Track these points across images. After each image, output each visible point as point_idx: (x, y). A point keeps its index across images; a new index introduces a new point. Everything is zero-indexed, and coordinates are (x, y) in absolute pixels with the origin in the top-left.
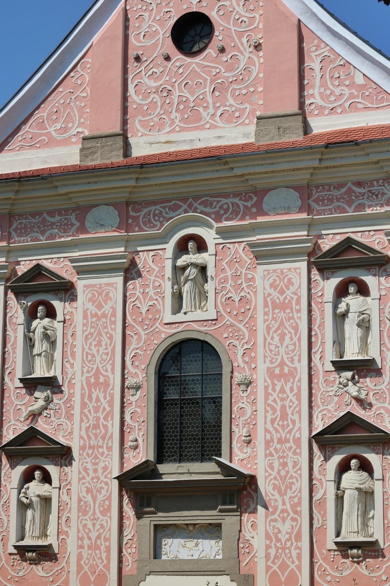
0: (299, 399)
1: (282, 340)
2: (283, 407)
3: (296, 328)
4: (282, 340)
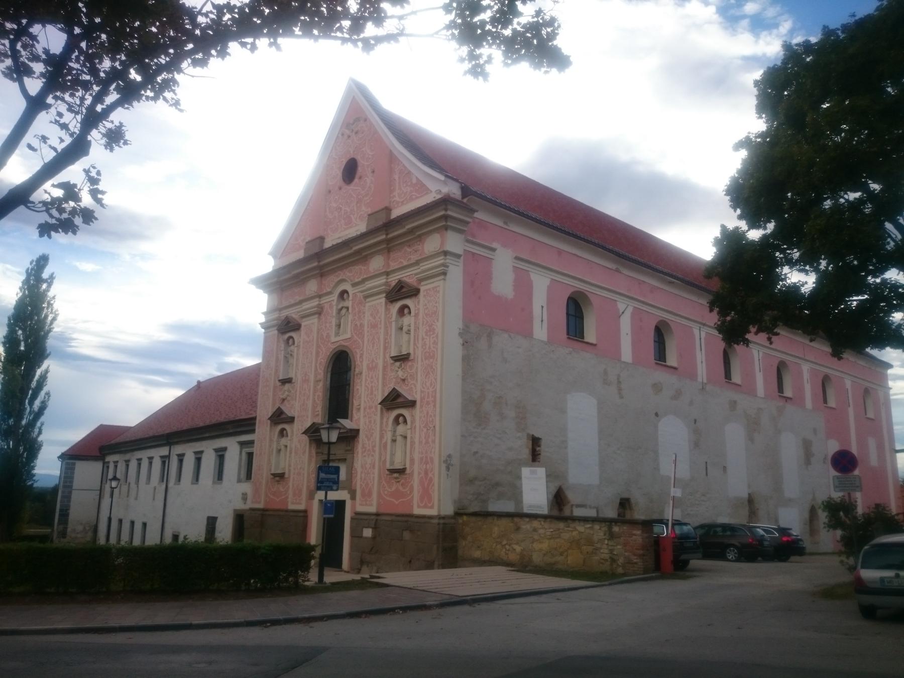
3: (379, 339)
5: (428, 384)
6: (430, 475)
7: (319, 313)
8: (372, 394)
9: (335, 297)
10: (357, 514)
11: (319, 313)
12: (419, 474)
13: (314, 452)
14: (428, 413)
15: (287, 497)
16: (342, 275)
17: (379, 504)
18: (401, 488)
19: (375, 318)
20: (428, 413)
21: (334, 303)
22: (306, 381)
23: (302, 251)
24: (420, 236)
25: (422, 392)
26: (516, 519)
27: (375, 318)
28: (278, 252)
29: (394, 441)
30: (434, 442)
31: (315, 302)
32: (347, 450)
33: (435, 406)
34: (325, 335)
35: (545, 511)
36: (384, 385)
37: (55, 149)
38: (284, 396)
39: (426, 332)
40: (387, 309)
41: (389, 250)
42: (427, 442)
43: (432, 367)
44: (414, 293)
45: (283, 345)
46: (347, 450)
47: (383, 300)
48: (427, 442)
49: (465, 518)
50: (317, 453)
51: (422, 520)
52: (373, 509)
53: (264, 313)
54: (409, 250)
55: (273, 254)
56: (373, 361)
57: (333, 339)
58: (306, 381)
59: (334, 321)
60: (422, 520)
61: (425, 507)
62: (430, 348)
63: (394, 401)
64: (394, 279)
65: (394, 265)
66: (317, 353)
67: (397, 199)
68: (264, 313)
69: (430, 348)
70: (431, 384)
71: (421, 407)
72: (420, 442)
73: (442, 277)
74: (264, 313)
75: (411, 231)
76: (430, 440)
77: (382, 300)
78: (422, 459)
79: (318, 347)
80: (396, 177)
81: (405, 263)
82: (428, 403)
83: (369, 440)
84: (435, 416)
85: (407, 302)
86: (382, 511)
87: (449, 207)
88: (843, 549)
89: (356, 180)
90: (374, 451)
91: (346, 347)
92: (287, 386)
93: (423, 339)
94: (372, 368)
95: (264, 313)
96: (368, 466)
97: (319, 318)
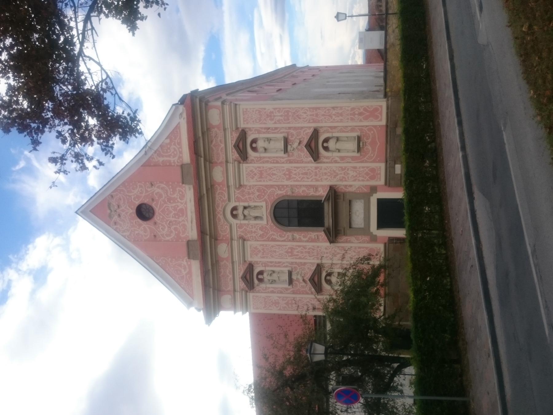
0: (299, 167)
1: (275, 174)
2: (302, 174)
3: (270, 169)
4: (275, 174)
5: (305, 116)
6: (362, 110)
7: (244, 240)
8: (306, 174)
10: (386, 184)
11: (244, 240)
12: (361, 121)
13: (344, 238)
14: (323, 115)
15: (375, 127)
16: (219, 209)
17: (380, 161)
18: (370, 140)
19: (255, 174)
20: (323, 115)
25: (309, 122)
26: (388, 47)
27: (255, 174)
28: (189, 301)
29: (339, 151)
30: (341, 108)
31: (235, 243)
32: (344, 200)
33: (319, 108)
34: (261, 233)
35: (383, 32)
37: (123, 113)
39: (272, 120)
40: (252, 162)
41: (210, 162)
42: (341, 115)
43: (294, 113)
46: (344, 200)
48: (341, 115)
49: (388, 90)
51: (389, 115)
52: (383, 166)
53: (235, 312)
55: (190, 304)
60: (389, 115)
61: (381, 113)
62: (281, 116)
63: (314, 146)
66: (274, 240)
67: (176, 158)
68: (235, 313)
69: (281, 116)
70: (305, 113)
71: (319, 122)
72: (341, 121)
73: (238, 106)
74: (235, 312)
75: (203, 133)
76: (340, 112)
78: (352, 119)
80: (161, 159)
81: (223, 145)
82: (317, 115)
83: (337, 175)
84: (325, 108)
86: (384, 158)
88: (413, 395)
89: (153, 205)
90: (345, 167)
91: (271, 206)
93: (275, 123)
94: (289, 175)
95: (235, 313)
96: (355, 174)
97: (248, 240)
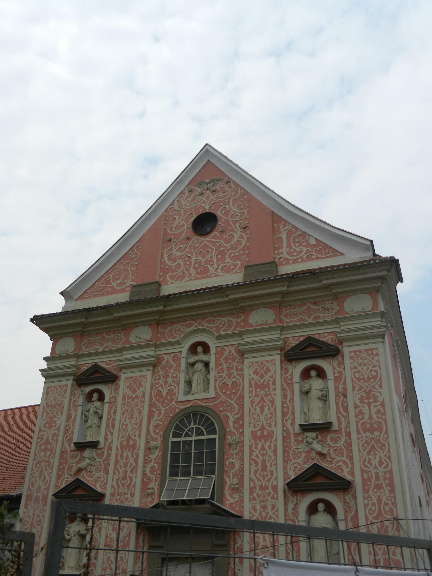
3: (273, 402)
8: (264, 468)
9: (185, 348)
14: (379, 500)
21: (184, 354)
22: (129, 445)
23: (128, 294)
24: (125, 325)
31: (150, 352)
36: (59, 477)
38: (82, 465)
41: (82, 334)
44: (111, 379)
45: (81, 401)
47: (277, 358)
50: (150, 547)
54: (106, 336)
56: (263, 428)
57: (181, 397)
58: (129, 445)
59: (182, 378)
62: (371, 417)
64: (87, 363)
65: (85, 350)
66: (151, 415)
69: (371, 417)
70: (381, 463)
77: (69, 382)
79: (152, 405)
85: (103, 388)
87: (227, 293)
92: (87, 453)
94: (263, 436)
97: (154, 372)
